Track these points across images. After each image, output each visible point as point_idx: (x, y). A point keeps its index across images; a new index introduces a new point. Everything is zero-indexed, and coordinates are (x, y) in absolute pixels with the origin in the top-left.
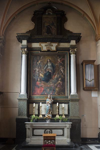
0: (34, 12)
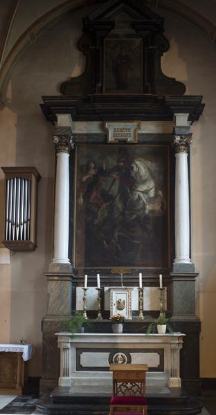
0: (163, 18)
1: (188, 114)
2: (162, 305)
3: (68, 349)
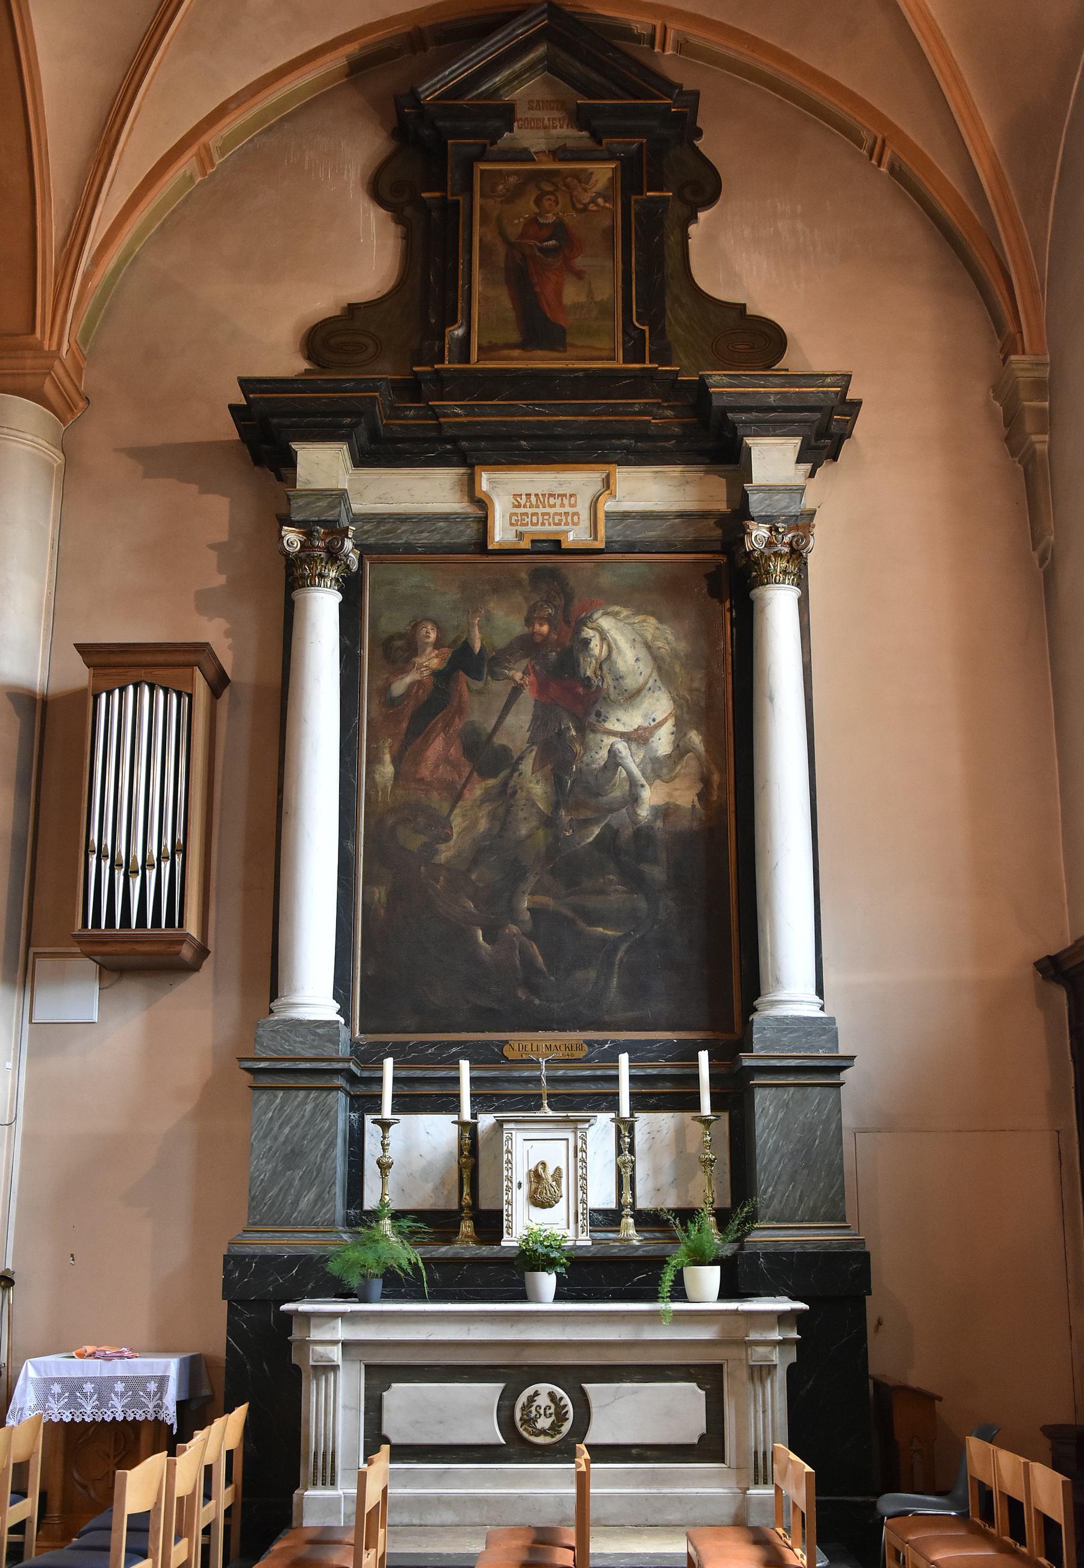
0: (696, 94)
1: (797, 441)
2: (707, 1191)
3: (335, 1368)
